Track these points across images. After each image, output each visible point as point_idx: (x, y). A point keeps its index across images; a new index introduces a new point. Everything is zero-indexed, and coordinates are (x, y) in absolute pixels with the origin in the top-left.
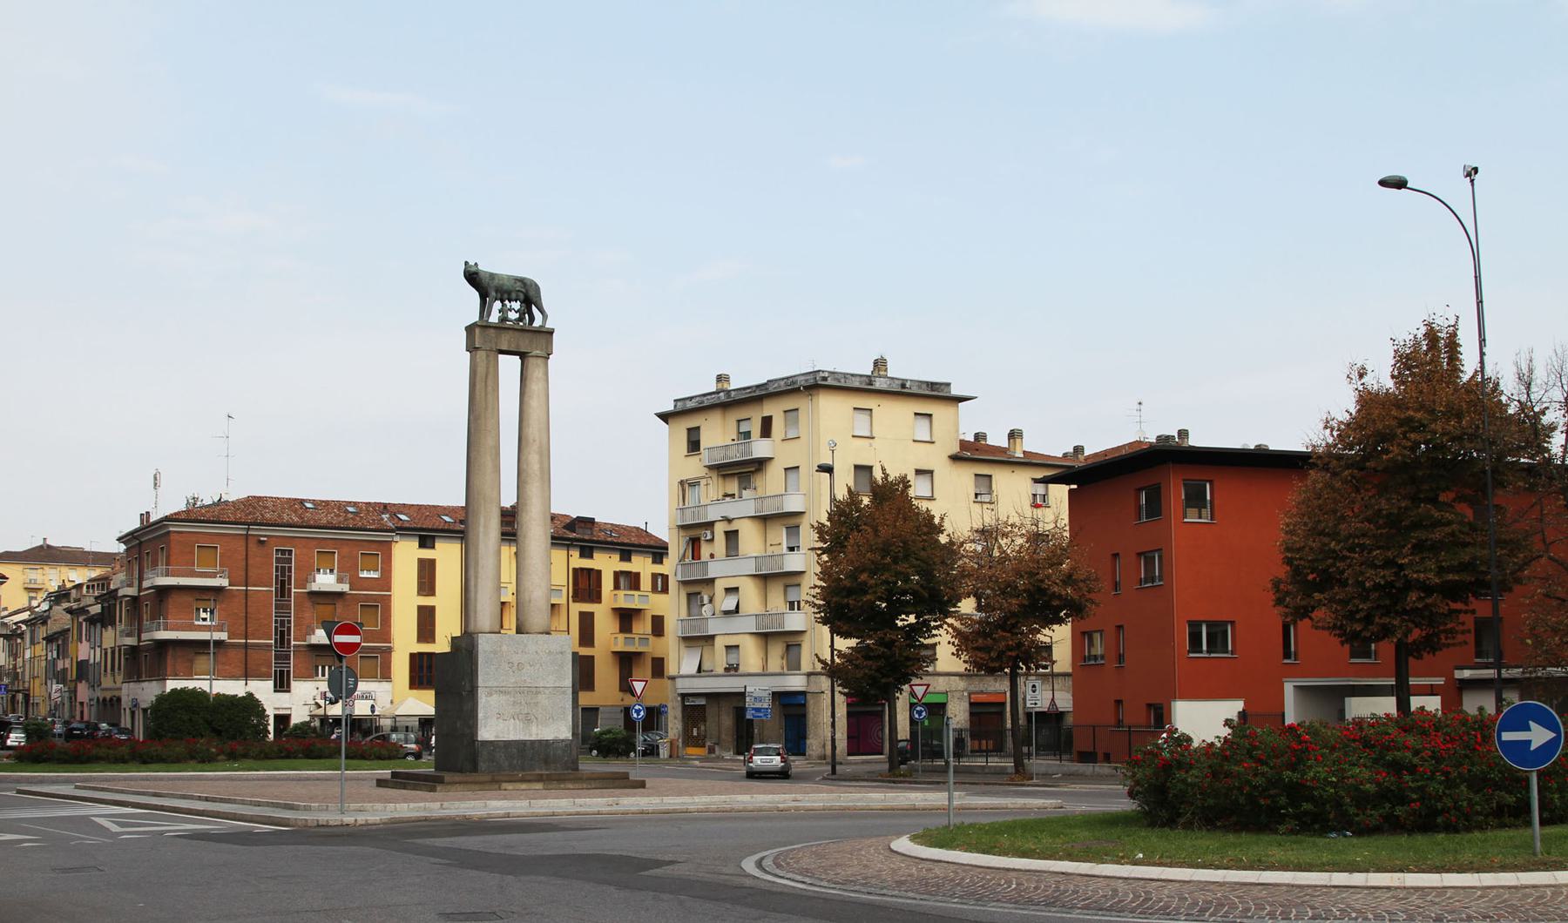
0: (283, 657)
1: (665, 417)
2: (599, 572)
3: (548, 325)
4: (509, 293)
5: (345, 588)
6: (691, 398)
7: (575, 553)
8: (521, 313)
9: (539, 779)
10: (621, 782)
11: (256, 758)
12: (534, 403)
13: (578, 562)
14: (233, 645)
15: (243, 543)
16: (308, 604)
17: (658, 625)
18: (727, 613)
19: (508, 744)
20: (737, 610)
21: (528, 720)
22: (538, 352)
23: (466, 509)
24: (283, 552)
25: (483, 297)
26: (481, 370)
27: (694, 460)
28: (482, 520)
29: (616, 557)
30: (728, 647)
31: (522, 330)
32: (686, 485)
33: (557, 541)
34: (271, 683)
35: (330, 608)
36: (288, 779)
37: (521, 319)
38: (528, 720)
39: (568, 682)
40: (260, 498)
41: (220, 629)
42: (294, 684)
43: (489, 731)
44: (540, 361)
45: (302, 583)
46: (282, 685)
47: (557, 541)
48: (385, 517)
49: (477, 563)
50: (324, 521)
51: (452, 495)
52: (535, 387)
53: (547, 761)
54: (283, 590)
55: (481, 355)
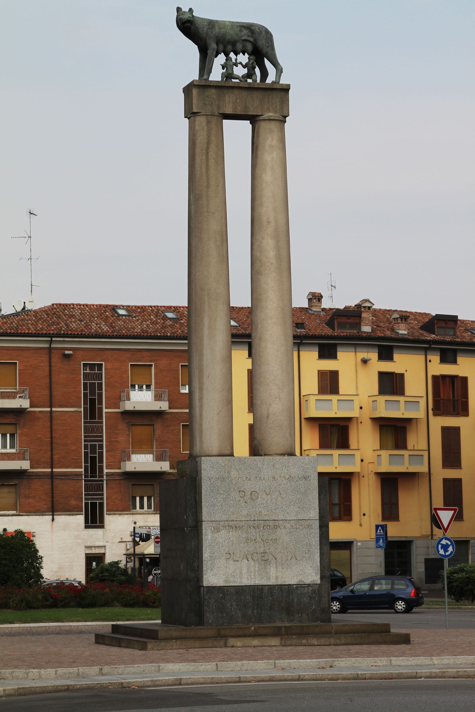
0: (94, 488)
2: (401, 376)
3: (283, 81)
4: (233, 43)
5: (164, 406)
7: (435, 358)
8: (250, 67)
9: (277, 633)
10: (382, 636)
11: (17, 608)
12: (268, 177)
13: (438, 368)
14: (38, 476)
15: (45, 358)
16: (122, 426)
19: (240, 590)
21: (264, 560)
24: (92, 367)
26: (201, 138)
28: (206, 321)
31: (251, 89)
33: (300, 341)
34: (80, 519)
35: (148, 429)
36: (47, 632)
38: (264, 560)
39: (314, 514)
40: (65, 307)
41: (19, 456)
42: (109, 519)
43: (216, 574)
44: (273, 126)
45: (115, 401)
46: (94, 520)
47: (300, 341)
49: (201, 371)
50: (138, 330)
51: (174, 294)
52: (269, 157)
53: (289, 611)
54: (93, 411)
55: (200, 120)
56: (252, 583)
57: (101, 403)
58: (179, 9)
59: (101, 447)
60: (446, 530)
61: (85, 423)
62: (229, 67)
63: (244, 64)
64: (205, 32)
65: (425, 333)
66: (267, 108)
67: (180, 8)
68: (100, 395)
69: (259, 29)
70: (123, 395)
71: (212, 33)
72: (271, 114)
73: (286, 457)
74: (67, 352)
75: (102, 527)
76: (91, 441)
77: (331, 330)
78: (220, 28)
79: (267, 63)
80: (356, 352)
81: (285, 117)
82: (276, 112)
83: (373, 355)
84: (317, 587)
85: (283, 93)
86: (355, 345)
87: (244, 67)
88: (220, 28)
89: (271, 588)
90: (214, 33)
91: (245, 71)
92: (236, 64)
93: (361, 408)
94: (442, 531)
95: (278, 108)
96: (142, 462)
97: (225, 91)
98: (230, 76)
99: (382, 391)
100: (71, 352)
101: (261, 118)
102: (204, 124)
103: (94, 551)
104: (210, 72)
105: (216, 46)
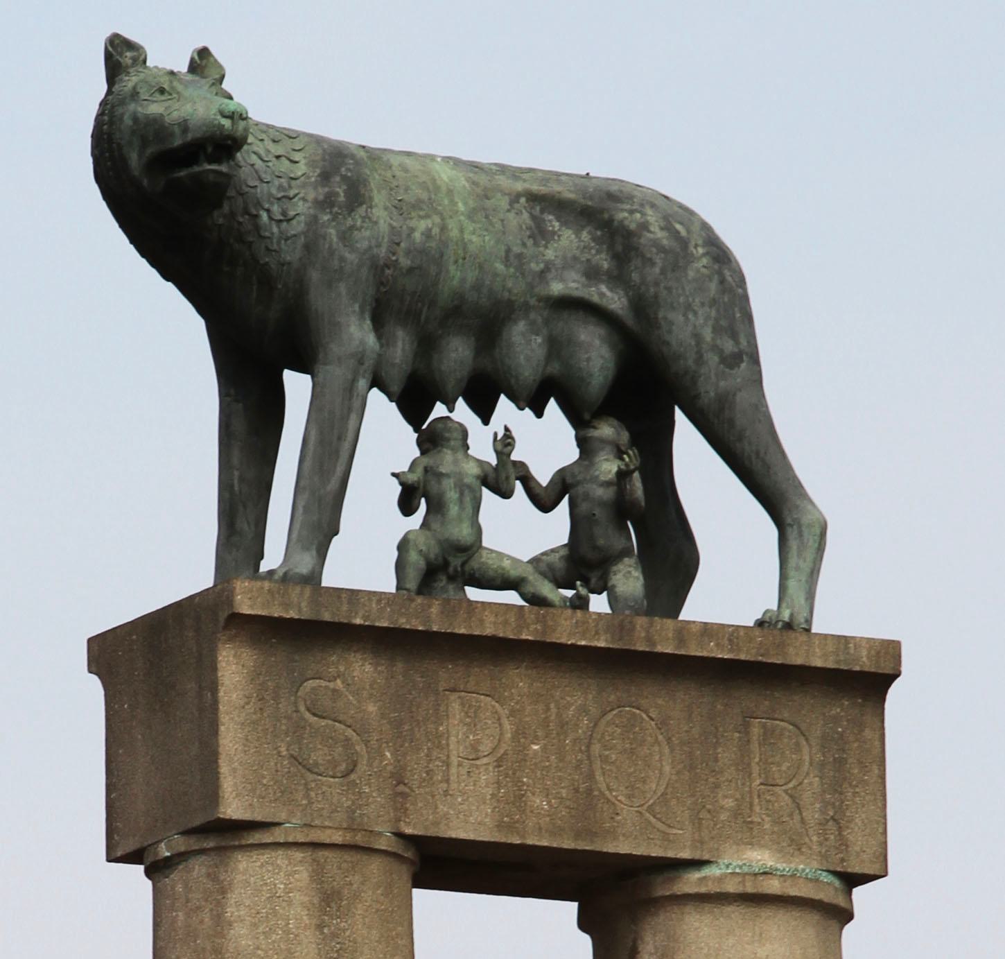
3: (844, 611)
4: (488, 321)
58: (120, 56)
62: (452, 495)
63: (543, 476)
64: (298, 226)
66: (736, 814)
67: (129, 45)
69: (668, 228)
71: (345, 237)
72: (761, 858)
78: (400, 208)
82: (794, 844)
85: (841, 708)
87: (543, 501)
88: (400, 208)
90: (363, 238)
95: (813, 814)
97: (445, 673)
98: (456, 562)
101: (691, 882)
102: (298, 910)
105: (371, 340)
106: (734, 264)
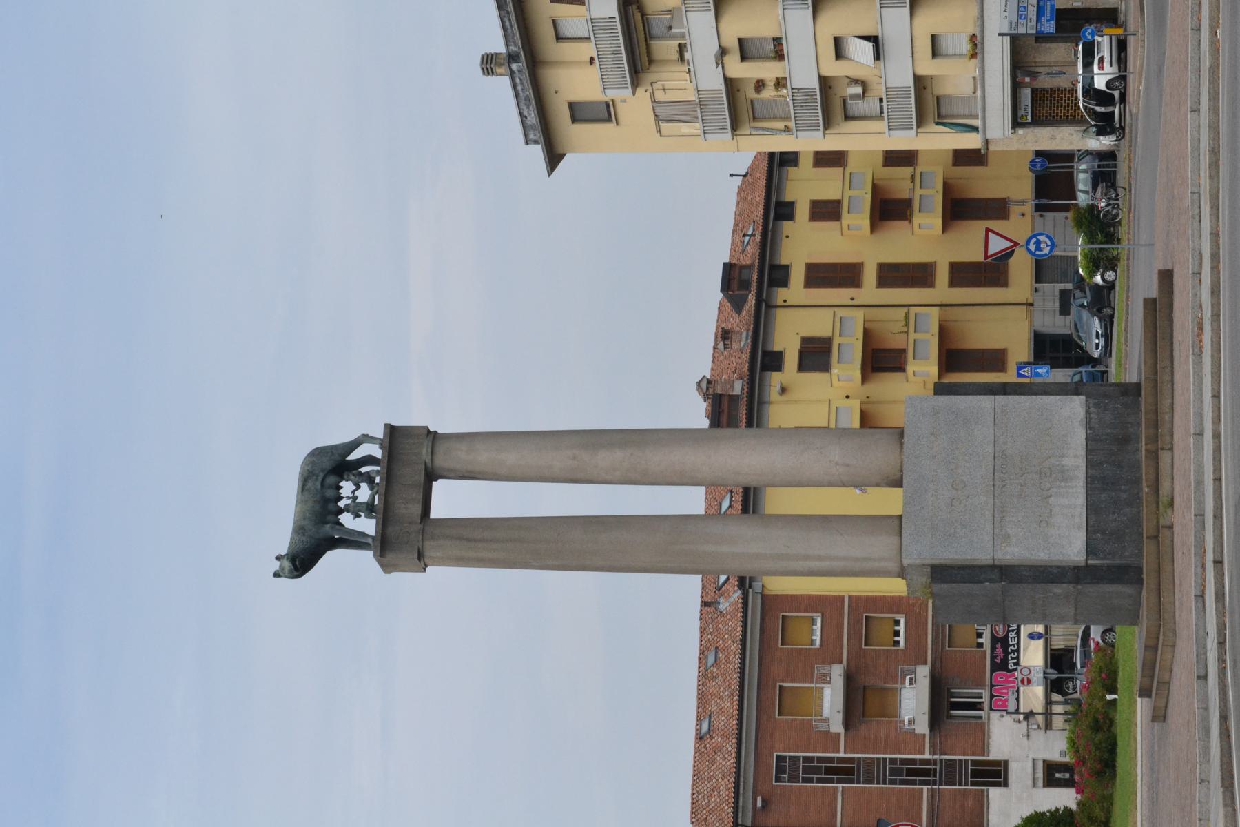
0: (951, 773)
1: (554, 159)
2: (805, 341)
3: (379, 433)
6: (523, 117)
7: (781, 294)
9: (1154, 456)
12: (511, 457)
17: (895, 158)
18: (877, 56)
19: (1092, 508)
20: (874, 40)
22: (425, 451)
23: (707, 486)
24: (780, 770)
25: (334, 543)
27: (622, 110)
29: (787, 226)
30: (935, 54)
31: (389, 478)
32: (664, 114)
34: (994, 793)
37: (369, 479)
42: (994, 755)
44: (441, 448)
46: (996, 774)
48: (724, 605)
54: (842, 771)
56: (1083, 491)
57: (831, 760)
58: (276, 575)
59: (893, 761)
60: (1016, 244)
61: (858, 782)
65: (746, 308)
68: (820, 760)
70: (821, 727)
72: (424, 451)
73: (905, 439)
74: (759, 804)
75: (1006, 763)
76: (884, 775)
77: (736, 406)
79: (353, 456)
80: (770, 403)
81: (429, 432)
83: (775, 379)
84: (1091, 401)
86: (761, 403)
87: (358, 487)
89: (1089, 464)
91: (364, 486)
92: (355, 498)
93: (847, 397)
94: (1017, 250)
96: (913, 703)
99: (825, 367)
100: (759, 799)
103: (1040, 775)
104: (363, 534)
106: (309, 467)
